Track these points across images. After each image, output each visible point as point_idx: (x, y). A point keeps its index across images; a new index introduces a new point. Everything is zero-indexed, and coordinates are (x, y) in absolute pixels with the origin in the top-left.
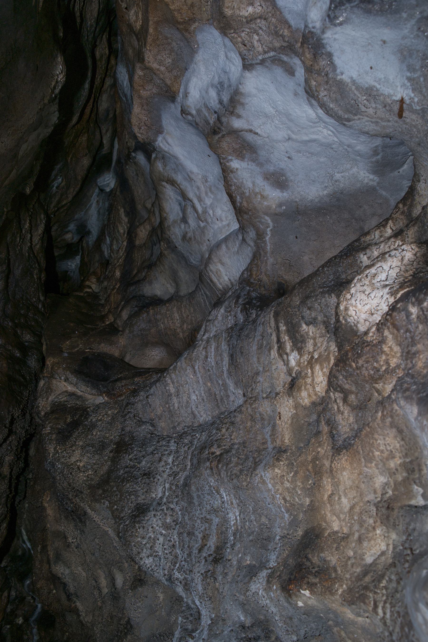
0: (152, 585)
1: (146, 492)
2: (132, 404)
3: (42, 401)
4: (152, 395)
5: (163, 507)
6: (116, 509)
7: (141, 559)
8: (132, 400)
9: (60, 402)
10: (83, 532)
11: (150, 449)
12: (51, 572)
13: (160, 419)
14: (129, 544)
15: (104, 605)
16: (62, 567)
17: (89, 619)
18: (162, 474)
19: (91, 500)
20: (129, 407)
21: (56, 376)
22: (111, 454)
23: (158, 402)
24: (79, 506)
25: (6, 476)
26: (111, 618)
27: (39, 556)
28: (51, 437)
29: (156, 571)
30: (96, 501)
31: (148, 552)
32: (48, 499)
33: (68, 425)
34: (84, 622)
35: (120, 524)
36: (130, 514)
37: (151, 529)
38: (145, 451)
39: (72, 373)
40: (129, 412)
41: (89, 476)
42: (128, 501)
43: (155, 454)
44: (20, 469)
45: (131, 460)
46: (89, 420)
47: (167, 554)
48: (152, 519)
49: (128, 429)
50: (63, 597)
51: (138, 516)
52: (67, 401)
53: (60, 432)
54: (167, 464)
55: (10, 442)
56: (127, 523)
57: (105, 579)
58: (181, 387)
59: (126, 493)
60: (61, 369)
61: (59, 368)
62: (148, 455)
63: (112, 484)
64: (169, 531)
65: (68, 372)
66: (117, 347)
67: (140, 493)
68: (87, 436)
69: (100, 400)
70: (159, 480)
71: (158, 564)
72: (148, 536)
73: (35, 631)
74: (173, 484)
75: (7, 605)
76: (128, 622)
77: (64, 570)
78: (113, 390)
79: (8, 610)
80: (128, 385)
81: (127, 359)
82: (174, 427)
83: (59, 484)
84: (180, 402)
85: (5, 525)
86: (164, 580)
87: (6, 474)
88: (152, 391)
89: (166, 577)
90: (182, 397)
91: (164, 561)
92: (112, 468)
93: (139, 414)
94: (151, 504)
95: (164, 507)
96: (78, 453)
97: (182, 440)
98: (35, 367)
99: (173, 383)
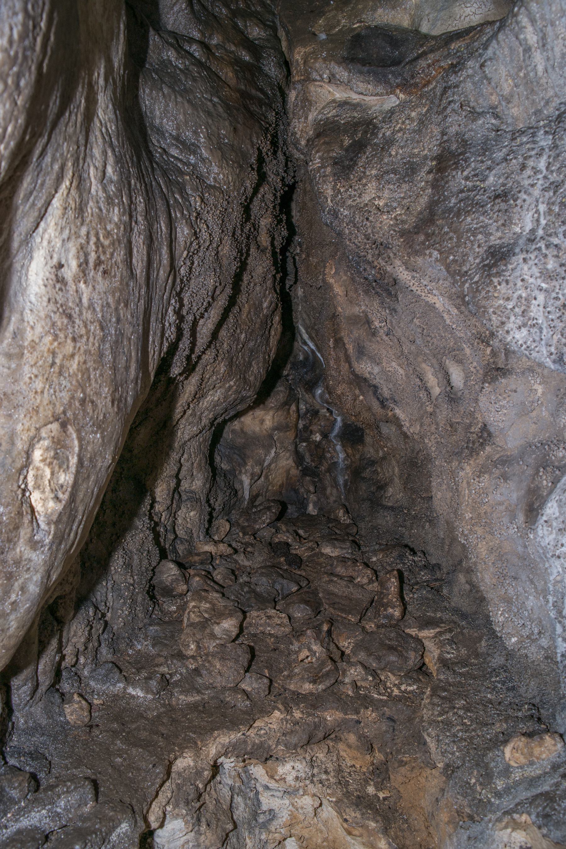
0: (523, 373)
1: (503, 225)
2: (455, 87)
3: (299, 122)
4: (490, 59)
5: (539, 245)
6: (453, 260)
7: (508, 332)
8: (453, 79)
9: (328, 118)
10: (394, 311)
11: (498, 155)
12: (353, 373)
13: (508, 103)
14: (484, 312)
15: (438, 410)
16: (369, 365)
18: (531, 190)
19: (408, 253)
20: (450, 92)
21: (315, 75)
22: (431, 177)
23: (503, 71)
24: (386, 272)
27: (332, 353)
28: (325, 172)
29: (534, 350)
30: (417, 253)
31: (519, 321)
32: (332, 273)
33: (347, 150)
34: (408, 433)
35: (464, 283)
36: (478, 264)
37: (520, 283)
38: (490, 159)
39: (339, 64)
40: (450, 102)
41: (398, 218)
42: (473, 245)
43: (511, 160)
44: (283, 239)
45: (467, 178)
46: (381, 135)
47: (552, 320)
48: (520, 266)
49: (453, 130)
50: (376, 405)
51: (495, 265)
52: (337, 116)
53: (336, 163)
54: (536, 171)
55: (263, 196)
56: (476, 279)
58: (549, 28)
59: (467, 232)
60: (320, 60)
61: (316, 59)
62: (498, 164)
63: (439, 222)
64: (554, 283)
65: (332, 63)
66: (405, 9)
67: (492, 229)
68: (382, 160)
69: (392, 101)
70: (524, 201)
71: (537, 339)
72: (515, 295)
73: (339, 447)
74: (553, 204)
75: (298, 420)
76: (485, 427)
77: (372, 368)
78: (413, 77)
79: (301, 426)
80: (438, 61)
81: (424, 29)
82: (538, 112)
83: (350, 240)
84: (548, 59)
86: (549, 363)
87: (264, 244)
88: (490, 52)
89: (553, 357)
90: (552, 49)
91: (548, 333)
92: (436, 198)
93: (469, 102)
94: (515, 244)
95: (542, 245)
97: (561, 125)
98: (277, 76)
99: (533, 21)
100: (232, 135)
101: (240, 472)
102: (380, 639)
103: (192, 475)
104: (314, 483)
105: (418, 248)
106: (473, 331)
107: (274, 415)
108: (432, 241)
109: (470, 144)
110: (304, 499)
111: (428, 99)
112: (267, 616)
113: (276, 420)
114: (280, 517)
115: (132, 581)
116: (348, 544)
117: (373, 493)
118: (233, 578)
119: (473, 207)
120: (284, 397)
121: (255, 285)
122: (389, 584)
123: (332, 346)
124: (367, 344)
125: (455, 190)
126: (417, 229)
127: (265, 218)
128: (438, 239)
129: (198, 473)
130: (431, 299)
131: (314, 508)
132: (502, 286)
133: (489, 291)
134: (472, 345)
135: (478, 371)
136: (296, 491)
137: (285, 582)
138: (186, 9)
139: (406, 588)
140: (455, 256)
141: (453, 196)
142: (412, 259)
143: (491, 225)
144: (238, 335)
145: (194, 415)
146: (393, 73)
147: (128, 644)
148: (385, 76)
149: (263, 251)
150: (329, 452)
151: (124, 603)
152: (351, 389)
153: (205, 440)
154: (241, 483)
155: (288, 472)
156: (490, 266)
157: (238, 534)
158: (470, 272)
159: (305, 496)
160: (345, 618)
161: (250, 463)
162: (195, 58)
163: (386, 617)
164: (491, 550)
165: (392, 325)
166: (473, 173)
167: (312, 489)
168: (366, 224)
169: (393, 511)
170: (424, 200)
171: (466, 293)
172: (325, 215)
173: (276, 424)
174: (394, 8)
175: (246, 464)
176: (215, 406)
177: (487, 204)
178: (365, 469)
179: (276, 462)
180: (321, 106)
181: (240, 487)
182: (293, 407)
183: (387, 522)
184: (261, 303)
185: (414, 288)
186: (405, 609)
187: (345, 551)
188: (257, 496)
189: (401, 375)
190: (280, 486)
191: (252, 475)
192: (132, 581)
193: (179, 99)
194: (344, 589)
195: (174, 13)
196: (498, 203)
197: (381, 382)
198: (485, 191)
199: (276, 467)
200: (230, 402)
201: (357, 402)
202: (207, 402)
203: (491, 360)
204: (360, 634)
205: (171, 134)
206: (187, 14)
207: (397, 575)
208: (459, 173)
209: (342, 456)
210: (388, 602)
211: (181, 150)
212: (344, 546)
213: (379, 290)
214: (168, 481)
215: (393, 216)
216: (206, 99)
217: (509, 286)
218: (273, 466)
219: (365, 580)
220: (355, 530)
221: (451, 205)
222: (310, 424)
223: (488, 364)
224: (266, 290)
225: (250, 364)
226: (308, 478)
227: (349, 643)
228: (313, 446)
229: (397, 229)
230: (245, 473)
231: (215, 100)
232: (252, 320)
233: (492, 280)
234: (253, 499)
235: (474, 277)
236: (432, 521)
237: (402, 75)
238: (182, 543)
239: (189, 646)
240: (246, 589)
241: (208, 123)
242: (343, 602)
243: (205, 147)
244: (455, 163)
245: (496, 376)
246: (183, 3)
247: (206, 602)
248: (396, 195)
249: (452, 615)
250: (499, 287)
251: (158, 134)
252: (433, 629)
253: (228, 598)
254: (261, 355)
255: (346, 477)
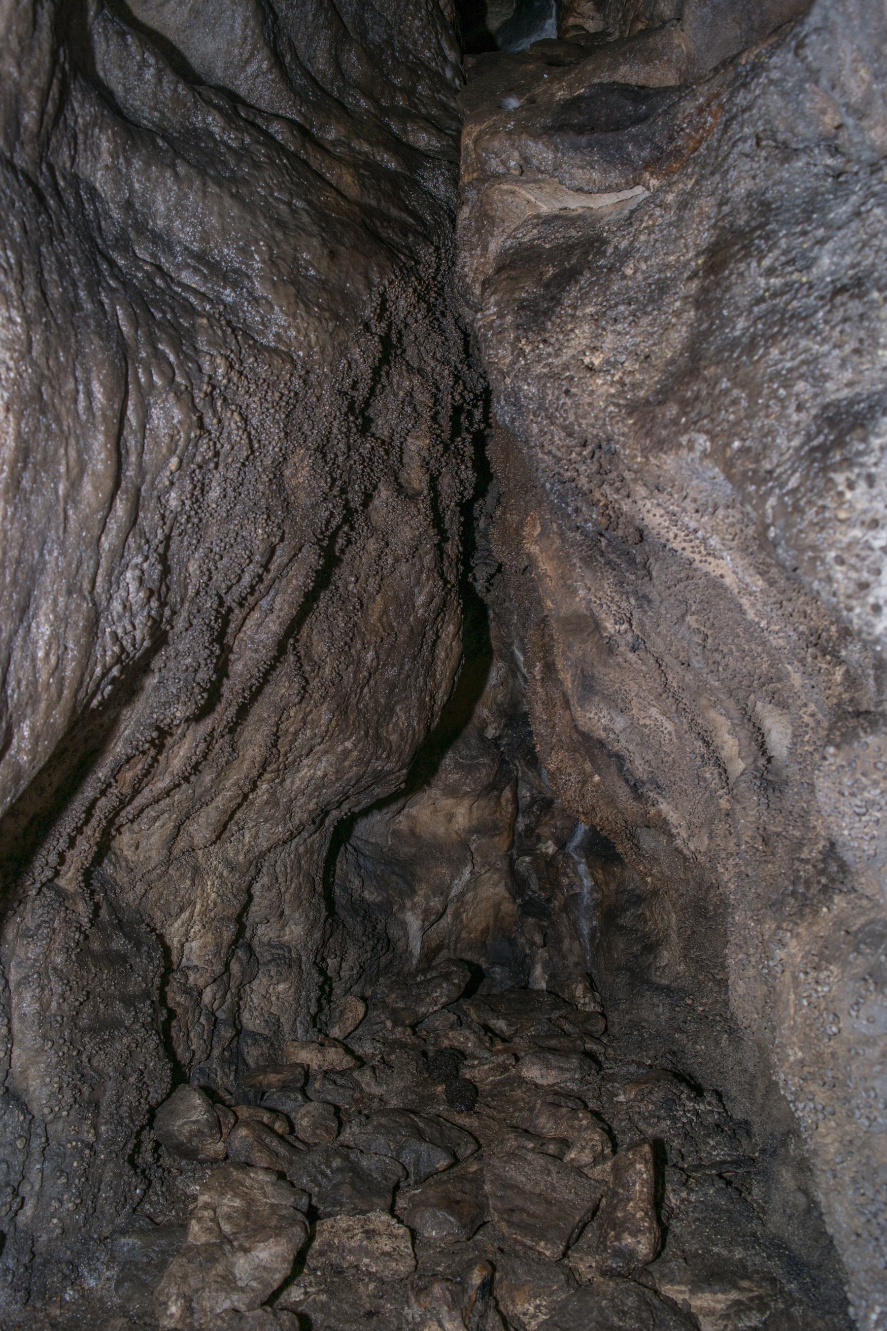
1: (857, 351)
3: (472, 256)
6: (740, 450)
14: (813, 560)
16: (605, 712)
17: (700, 843)
24: (620, 514)
25: (419, 493)
26: (765, 842)
27: (540, 690)
30: (661, 445)
32: (535, 534)
34: (686, 851)
35: (764, 498)
36: (798, 450)
38: (822, 225)
39: (536, 137)
42: (784, 408)
45: (770, 272)
46: (610, 250)
50: (623, 793)
57: (733, 732)
59: (771, 380)
67: (831, 365)
68: (608, 288)
73: (582, 868)
77: (612, 719)
78: (671, 139)
85: (451, 628)
87: (416, 485)
92: (705, 326)
96: (582, 334)
100: (325, 263)
101: (403, 907)
102: (601, 1310)
103: (283, 912)
104: (541, 928)
105: (664, 433)
106: (802, 628)
107: (471, 806)
108: (693, 415)
109: (778, 208)
110: (526, 955)
111: (696, 164)
112: (366, 1232)
113: (475, 814)
114: (469, 992)
115: (91, 1138)
116: (575, 1061)
117: (636, 957)
118: (334, 1125)
119: (784, 325)
120: (488, 775)
121: (397, 560)
122: (631, 1176)
123: (538, 678)
124: (599, 671)
125: (744, 302)
126: (663, 395)
127: (417, 438)
128: (706, 409)
129: (294, 911)
130: (714, 567)
131: (544, 972)
132: (858, 491)
133: (824, 508)
134: (802, 661)
135: (818, 722)
136: (512, 942)
137: (424, 1147)
138: (270, 70)
139: (672, 1176)
140: (743, 440)
141: (739, 316)
142: (653, 460)
143: (825, 355)
144: (359, 653)
145: (273, 801)
146: (634, 139)
147: (65, 1277)
148: (620, 148)
149: (413, 497)
150: (565, 874)
151: (68, 1185)
152: (575, 761)
153: (310, 851)
154: (404, 925)
155: (497, 907)
156: (825, 450)
157: (383, 1022)
158: (778, 471)
159: (528, 951)
160: (531, 1248)
161: (422, 891)
162: (276, 141)
163: (618, 1253)
164: (849, 1146)
165: (643, 630)
166: (783, 259)
167: (538, 939)
168: (564, 404)
169: (668, 996)
170: (679, 336)
171: (769, 521)
172: (502, 408)
173: (474, 822)
174: (648, 61)
175: (413, 892)
176: (319, 788)
177: (816, 312)
178: (625, 910)
179: (475, 889)
180: (513, 227)
181: (401, 933)
182: (507, 793)
183: (658, 1016)
184: (411, 596)
185: (676, 545)
186: (664, 1230)
187: (568, 1075)
188: (439, 948)
189: (670, 734)
190: (482, 932)
191: (427, 912)
192: (91, 1138)
193: (213, 189)
194: (539, 1177)
195: (247, 78)
196: (843, 304)
197: (631, 748)
198: (810, 288)
199: (475, 898)
200: (350, 780)
201: (589, 787)
202: (301, 779)
203: (846, 696)
204: (561, 1288)
205: (186, 248)
206: (273, 81)
207: (649, 1156)
208: (754, 264)
209: (588, 883)
210: (626, 1219)
211: (205, 276)
212: (567, 1066)
213: (612, 556)
214: (216, 928)
215: (616, 378)
216: (276, 199)
217: (875, 492)
218: (469, 896)
219: (586, 1157)
220: (601, 1026)
221: (737, 333)
222: (538, 822)
223: (838, 705)
224: (421, 572)
225: (390, 711)
226: (531, 920)
227: (537, 1307)
228: (542, 864)
229: (622, 402)
230: (413, 908)
231: (299, 204)
232: (391, 627)
233: (831, 480)
234: (430, 954)
235: (788, 480)
236: (733, 1031)
237: (651, 140)
238: (255, 1042)
239: (167, 1308)
240: (337, 1163)
241: (273, 237)
242: (532, 1208)
243: (261, 277)
244: (744, 247)
245: (854, 728)
246: (262, 60)
247: (236, 1195)
248: (628, 341)
249: (769, 1257)
250: (849, 495)
251: (154, 243)
252: (724, 1292)
253: (293, 1185)
254: (414, 696)
255: (595, 923)
